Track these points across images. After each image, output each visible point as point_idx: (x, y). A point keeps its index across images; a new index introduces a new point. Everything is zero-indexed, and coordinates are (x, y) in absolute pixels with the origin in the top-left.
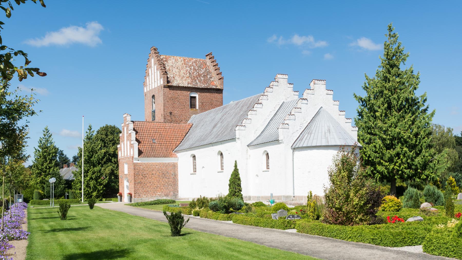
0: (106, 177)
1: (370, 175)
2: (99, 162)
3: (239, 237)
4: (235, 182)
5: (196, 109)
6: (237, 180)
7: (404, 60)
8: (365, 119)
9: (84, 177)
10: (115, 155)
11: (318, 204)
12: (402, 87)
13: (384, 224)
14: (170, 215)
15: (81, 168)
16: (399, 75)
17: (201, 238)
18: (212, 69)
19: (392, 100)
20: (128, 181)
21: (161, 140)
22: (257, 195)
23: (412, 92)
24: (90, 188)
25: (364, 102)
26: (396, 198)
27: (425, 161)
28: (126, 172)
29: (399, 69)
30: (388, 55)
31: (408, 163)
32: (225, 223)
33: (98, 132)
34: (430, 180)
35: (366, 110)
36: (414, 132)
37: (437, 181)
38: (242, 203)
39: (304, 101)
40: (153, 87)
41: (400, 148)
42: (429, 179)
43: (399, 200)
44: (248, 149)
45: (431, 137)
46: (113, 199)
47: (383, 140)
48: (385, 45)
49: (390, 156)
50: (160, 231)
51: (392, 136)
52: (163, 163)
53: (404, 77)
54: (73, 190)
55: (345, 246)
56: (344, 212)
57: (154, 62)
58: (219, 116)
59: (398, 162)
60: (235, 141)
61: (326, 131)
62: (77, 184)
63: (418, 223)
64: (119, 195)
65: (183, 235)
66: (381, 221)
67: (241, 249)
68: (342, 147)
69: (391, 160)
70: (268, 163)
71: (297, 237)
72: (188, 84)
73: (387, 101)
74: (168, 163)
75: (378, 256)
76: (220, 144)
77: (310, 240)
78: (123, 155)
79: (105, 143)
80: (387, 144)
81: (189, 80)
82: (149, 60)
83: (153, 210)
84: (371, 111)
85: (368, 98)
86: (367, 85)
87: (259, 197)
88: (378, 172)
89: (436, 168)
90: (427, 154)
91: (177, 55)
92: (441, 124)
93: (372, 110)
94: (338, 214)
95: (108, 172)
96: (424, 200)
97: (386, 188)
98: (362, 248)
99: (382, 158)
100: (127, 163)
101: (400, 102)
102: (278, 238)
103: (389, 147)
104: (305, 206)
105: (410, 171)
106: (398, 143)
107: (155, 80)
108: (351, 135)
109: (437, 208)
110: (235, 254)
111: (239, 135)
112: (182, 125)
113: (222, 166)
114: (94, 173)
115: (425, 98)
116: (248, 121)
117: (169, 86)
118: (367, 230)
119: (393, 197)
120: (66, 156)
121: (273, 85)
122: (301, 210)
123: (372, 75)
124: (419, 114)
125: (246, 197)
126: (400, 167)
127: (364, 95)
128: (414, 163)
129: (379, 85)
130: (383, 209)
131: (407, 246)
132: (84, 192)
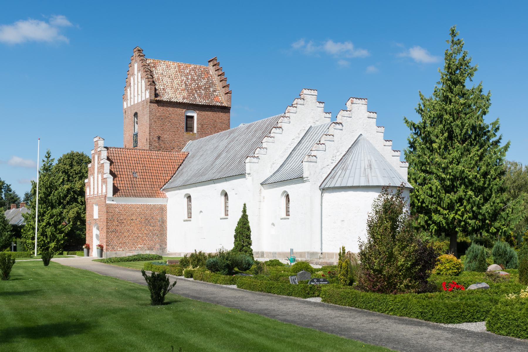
0: (70, 222)
1: (423, 227)
2: (60, 201)
3: (244, 307)
4: (243, 232)
5: (194, 134)
6: (246, 230)
7: (471, 74)
8: (419, 152)
9: (39, 221)
10: (82, 193)
11: (352, 264)
12: (468, 111)
13: (437, 293)
14: (150, 275)
15: (35, 209)
16: (463, 95)
17: (191, 308)
18: (216, 79)
19: (454, 127)
20: (98, 229)
21: (146, 173)
22: (272, 251)
23: (480, 118)
24: (47, 237)
25: (417, 129)
26: (455, 258)
27: (496, 210)
28: (96, 216)
29: (464, 86)
30: (449, 68)
31: (473, 212)
32: (226, 288)
33: (60, 161)
34: (501, 236)
35: (420, 140)
36: (482, 171)
37: (510, 236)
38: (251, 262)
39: (338, 126)
40: (136, 102)
41: (464, 191)
42: (500, 234)
43: (460, 261)
44: (262, 188)
45: (504, 178)
46: (77, 252)
47: (442, 180)
48: (446, 54)
49: (449, 202)
50: (136, 298)
51: (453, 176)
52: (147, 205)
53: (471, 97)
54: (23, 240)
55: (384, 321)
56: (385, 275)
57: (138, 68)
58: (225, 142)
59: (460, 210)
60: (245, 177)
61: (366, 167)
62: (29, 231)
63: (482, 292)
64: (86, 247)
65: (167, 303)
66: (434, 288)
67: (245, 324)
68: (385, 189)
69: (451, 207)
70: (287, 208)
71: (321, 309)
72: (184, 98)
73: (448, 128)
74: (154, 205)
75: (427, 335)
76: (224, 181)
77: (338, 313)
78: (92, 193)
79: (69, 176)
80: (446, 185)
81: (185, 94)
82: (131, 65)
83: (130, 268)
84: (426, 142)
85: (423, 125)
86: (422, 107)
87: (275, 253)
88: (434, 222)
89: (509, 219)
90: (498, 201)
91: (169, 59)
92: (517, 161)
93: (428, 140)
94: (377, 277)
95: (73, 216)
96: (492, 261)
97: (445, 244)
98: (407, 324)
99: (439, 205)
100: (97, 204)
101: (464, 131)
102: (297, 309)
103: (449, 190)
104: (335, 267)
105: (475, 223)
106: (460, 185)
107: (138, 92)
108: (399, 173)
109: (508, 272)
110: (236, 331)
111: (250, 170)
112: (174, 153)
113: (226, 211)
114: (52, 217)
115: (497, 126)
116: (262, 151)
117: (157, 101)
118: (415, 301)
119: (451, 256)
120: (14, 192)
121: (297, 104)
122: (329, 272)
123: (429, 94)
124: (489, 147)
125: (257, 253)
126: (462, 216)
127: (418, 120)
128: (481, 211)
129: (437, 107)
130: (438, 271)
131: (466, 322)
132: (38, 242)
